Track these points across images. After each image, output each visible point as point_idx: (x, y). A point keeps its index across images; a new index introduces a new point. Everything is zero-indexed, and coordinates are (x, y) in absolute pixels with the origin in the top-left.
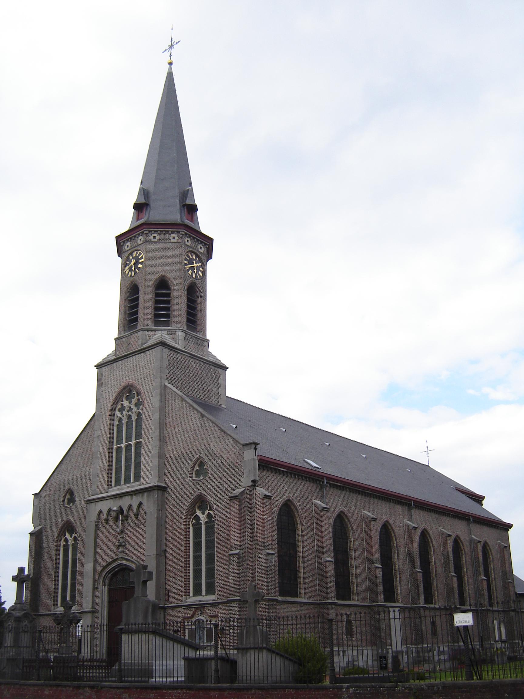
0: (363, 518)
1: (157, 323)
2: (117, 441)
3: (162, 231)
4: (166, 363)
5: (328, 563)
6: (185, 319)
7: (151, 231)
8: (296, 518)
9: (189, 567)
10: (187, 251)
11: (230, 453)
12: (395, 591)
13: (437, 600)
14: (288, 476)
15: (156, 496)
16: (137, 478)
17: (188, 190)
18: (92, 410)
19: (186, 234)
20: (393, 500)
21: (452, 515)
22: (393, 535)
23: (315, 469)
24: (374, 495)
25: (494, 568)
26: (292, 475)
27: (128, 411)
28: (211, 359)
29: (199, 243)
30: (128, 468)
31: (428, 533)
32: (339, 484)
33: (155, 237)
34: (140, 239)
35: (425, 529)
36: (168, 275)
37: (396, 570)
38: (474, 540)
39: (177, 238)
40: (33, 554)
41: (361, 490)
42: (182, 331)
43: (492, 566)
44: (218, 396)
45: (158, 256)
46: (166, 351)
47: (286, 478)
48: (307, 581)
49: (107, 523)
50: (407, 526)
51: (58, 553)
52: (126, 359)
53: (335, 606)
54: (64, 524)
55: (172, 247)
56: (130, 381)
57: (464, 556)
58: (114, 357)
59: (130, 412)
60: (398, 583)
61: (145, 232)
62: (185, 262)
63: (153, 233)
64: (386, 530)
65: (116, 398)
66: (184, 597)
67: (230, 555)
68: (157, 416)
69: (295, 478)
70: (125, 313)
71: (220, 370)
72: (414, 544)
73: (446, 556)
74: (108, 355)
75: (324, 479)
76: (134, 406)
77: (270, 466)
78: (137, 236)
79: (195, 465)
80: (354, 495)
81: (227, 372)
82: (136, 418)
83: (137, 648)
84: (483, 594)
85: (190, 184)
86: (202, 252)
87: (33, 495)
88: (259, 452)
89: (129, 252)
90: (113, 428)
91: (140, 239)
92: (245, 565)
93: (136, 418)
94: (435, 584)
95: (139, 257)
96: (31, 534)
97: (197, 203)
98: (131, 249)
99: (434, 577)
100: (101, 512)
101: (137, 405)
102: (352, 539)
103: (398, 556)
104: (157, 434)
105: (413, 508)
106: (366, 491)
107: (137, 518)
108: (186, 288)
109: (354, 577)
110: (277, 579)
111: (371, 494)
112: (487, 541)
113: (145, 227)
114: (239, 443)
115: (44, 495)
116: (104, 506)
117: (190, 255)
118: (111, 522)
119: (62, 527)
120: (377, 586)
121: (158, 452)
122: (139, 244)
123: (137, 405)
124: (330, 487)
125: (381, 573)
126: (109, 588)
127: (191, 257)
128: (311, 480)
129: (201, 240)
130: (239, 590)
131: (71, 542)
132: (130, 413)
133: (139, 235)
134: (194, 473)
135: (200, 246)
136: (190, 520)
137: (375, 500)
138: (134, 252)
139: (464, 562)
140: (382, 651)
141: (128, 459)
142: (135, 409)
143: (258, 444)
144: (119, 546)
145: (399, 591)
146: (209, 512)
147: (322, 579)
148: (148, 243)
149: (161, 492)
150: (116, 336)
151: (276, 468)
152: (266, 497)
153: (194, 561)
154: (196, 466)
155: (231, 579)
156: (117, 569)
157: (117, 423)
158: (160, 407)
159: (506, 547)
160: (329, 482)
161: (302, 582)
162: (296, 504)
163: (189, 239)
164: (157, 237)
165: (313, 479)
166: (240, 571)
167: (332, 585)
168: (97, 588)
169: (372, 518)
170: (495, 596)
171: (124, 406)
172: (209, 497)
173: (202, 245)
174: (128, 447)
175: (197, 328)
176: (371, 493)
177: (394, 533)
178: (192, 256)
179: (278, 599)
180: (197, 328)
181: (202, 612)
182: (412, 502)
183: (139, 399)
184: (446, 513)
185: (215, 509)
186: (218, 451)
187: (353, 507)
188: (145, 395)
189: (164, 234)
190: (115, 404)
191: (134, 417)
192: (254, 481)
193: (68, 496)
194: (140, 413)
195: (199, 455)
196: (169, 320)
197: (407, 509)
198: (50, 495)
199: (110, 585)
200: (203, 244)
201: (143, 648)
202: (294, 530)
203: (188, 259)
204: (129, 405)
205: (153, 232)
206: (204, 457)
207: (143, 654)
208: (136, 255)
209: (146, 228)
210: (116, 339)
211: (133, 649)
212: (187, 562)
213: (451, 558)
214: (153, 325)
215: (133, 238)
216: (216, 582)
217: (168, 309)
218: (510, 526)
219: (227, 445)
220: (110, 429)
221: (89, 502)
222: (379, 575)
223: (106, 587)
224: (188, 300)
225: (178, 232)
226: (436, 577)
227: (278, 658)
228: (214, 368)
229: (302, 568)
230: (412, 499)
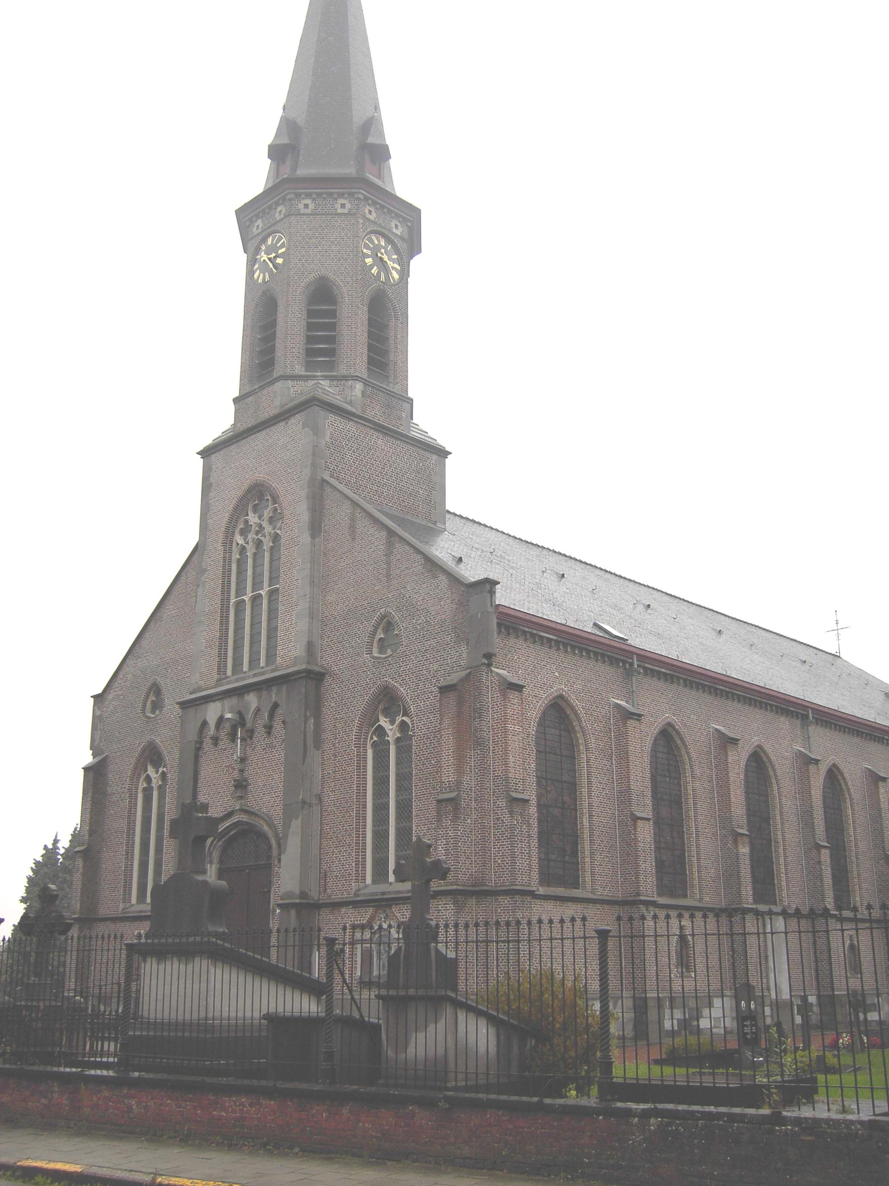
0: (712, 739)
3: (321, 194)
6: (365, 358)
8: (575, 732)
9: (365, 826)
10: (369, 230)
12: (776, 882)
14: (558, 649)
15: (304, 690)
16: (271, 656)
18: (193, 538)
19: (366, 199)
20: (771, 706)
22: (771, 773)
24: (733, 694)
26: (567, 648)
27: (257, 533)
28: (414, 434)
31: (842, 774)
32: (664, 670)
33: (306, 205)
34: (280, 212)
35: (834, 765)
36: (331, 276)
39: (348, 206)
40: (89, 806)
41: (707, 683)
45: (314, 240)
48: (598, 857)
53: (655, 907)
54: (144, 750)
59: (260, 535)
60: (782, 867)
61: (288, 197)
63: (303, 199)
65: (236, 509)
66: (353, 884)
67: (439, 801)
69: (574, 654)
72: (813, 792)
74: (223, 433)
75: (632, 658)
76: (267, 522)
77: (521, 627)
80: (694, 693)
81: (449, 461)
83: (174, 990)
87: (91, 697)
89: (260, 237)
91: (280, 212)
92: (469, 821)
94: (855, 872)
95: (278, 245)
96: (86, 769)
97: (389, 141)
98: (262, 232)
99: (854, 859)
101: (271, 520)
102: (689, 779)
103: (781, 814)
106: (718, 687)
107: (269, 733)
109: (694, 853)
110: (535, 853)
111: (727, 693)
117: (374, 238)
118: (224, 743)
122: (278, 219)
123: (271, 520)
124: (646, 674)
126: (219, 869)
127: (376, 242)
128: (606, 660)
129: (325, 191)
131: (156, 782)
132: (259, 536)
134: (375, 645)
136: (367, 736)
137: (736, 704)
138: (268, 236)
140: (748, 1005)
142: (268, 529)
145: (784, 883)
146: (402, 720)
147: (628, 855)
148: (293, 217)
151: (535, 632)
153: (374, 815)
154: (380, 630)
156: (233, 832)
157: (238, 557)
160: (643, 664)
161: (587, 860)
162: (575, 704)
163: (372, 209)
165: (610, 657)
166: (459, 834)
167: (647, 865)
171: (250, 523)
172: (402, 689)
173: (399, 221)
174: (256, 599)
175: (388, 377)
176: (728, 690)
177: (774, 771)
178: (379, 241)
179: (534, 891)
180: (388, 377)
181: (387, 915)
182: (810, 712)
183: (275, 510)
184: (876, 736)
185: (413, 712)
186: (420, 599)
189: (325, 198)
191: (267, 543)
193: (152, 698)
194: (278, 534)
195: (384, 609)
196: (333, 359)
198: (122, 697)
199: (221, 862)
200: (401, 219)
201: (189, 990)
203: (371, 246)
204: (259, 521)
206: (393, 613)
207: (188, 1005)
208: (272, 242)
209: (289, 189)
210: (236, 401)
211: (167, 992)
214: (303, 369)
215: (267, 211)
217: (332, 340)
220: (224, 567)
221: (184, 705)
223: (214, 866)
224: (371, 323)
225: (351, 195)
226: (857, 858)
227: (483, 1023)
229: (586, 831)
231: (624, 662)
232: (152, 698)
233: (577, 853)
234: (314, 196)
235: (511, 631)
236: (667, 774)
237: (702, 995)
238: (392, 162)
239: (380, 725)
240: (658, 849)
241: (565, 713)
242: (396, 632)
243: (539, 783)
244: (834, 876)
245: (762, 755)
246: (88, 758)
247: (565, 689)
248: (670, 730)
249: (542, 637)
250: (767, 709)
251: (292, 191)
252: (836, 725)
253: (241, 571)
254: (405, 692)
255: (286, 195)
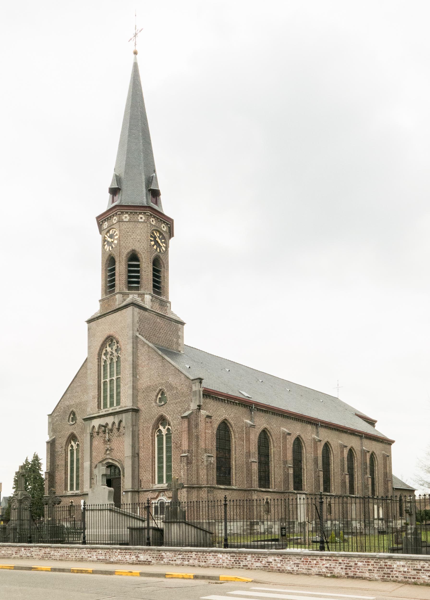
1: (130, 288)
2: (104, 377)
4: (137, 319)
5: (253, 464)
6: (152, 286)
7: (123, 212)
8: (231, 432)
9: (155, 464)
11: (182, 386)
13: (333, 490)
16: (118, 403)
17: (153, 177)
18: (84, 355)
19: (151, 215)
20: (305, 421)
21: (349, 432)
22: (303, 445)
23: (247, 398)
25: (378, 470)
28: (172, 316)
29: (162, 223)
30: (112, 397)
31: (330, 445)
32: (264, 409)
33: (126, 217)
34: (115, 219)
35: (327, 442)
36: (137, 250)
37: (304, 469)
38: (364, 450)
39: (144, 218)
42: (150, 294)
43: (377, 468)
44: (178, 344)
45: (129, 233)
46: (137, 310)
47: (224, 404)
48: (238, 475)
49: (98, 435)
50: (314, 439)
51: (66, 455)
52: (108, 316)
54: (70, 436)
55: (140, 226)
56: (112, 333)
57: (356, 461)
58: (99, 315)
61: (118, 213)
62: (151, 238)
64: (298, 442)
67: (181, 457)
68: (130, 358)
70: (106, 280)
71: (180, 326)
72: (318, 452)
73: (342, 460)
75: (252, 405)
77: (212, 395)
78: (112, 217)
79: (158, 394)
81: (185, 326)
82: (117, 360)
84: (368, 488)
85: (154, 171)
86: (165, 230)
88: (204, 385)
89: (107, 230)
90: (101, 367)
91: (115, 219)
93: (117, 360)
94: (333, 479)
98: (108, 227)
100: (94, 427)
102: (272, 447)
103: (306, 459)
104: (131, 372)
105: (363, 438)
107: (118, 431)
108: (152, 261)
111: (288, 417)
112: (375, 452)
113: (118, 208)
114: (189, 379)
115: (55, 415)
116: (96, 423)
119: (69, 438)
120: (288, 479)
121: (132, 384)
125: (292, 471)
129: (134, 211)
130: (188, 480)
131: (75, 447)
133: (113, 215)
135: (163, 225)
139: (356, 465)
141: (111, 390)
142: (115, 354)
143: (202, 379)
144: (107, 450)
149: (135, 413)
150: (100, 299)
151: (216, 396)
152: (208, 417)
155: (182, 473)
158: (133, 352)
159: (388, 456)
163: (154, 219)
164: (128, 218)
165: (244, 405)
167: (255, 478)
168: (93, 479)
169: (288, 433)
170: (377, 489)
173: (165, 225)
174: (111, 381)
183: (118, 346)
187: (274, 425)
188: (122, 342)
190: (101, 350)
191: (115, 360)
192: (199, 406)
193: (72, 416)
194: (119, 356)
197: (315, 428)
200: (166, 224)
202: (229, 441)
205: (124, 213)
212: (153, 461)
213: (346, 462)
215: (109, 218)
216: (173, 474)
218: (393, 442)
219: (181, 380)
221: (85, 420)
222: (290, 472)
224: (154, 270)
225: (145, 213)
228: (175, 323)
230: (253, 402)
231: (249, 406)
232: (72, 416)
233: (230, 473)
234: (129, 213)
235: (208, 397)
236: (264, 445)
237: (109, 471)
238: (161, 196)
239: (159, 429)
240: (260, 472)
241: (227, 425)
242: (165, 396)
243: (217, 450)
244: (324, 481)
245: (300, 438)
246: (47, 438)
247: (227, 417)
248: (266, 430)
249: (219, 399)
250: (303, 422)
251: (120, 211)
252: (329, 427)
253: (105, 370)
254: (169, 418)
255: (117, 212)
